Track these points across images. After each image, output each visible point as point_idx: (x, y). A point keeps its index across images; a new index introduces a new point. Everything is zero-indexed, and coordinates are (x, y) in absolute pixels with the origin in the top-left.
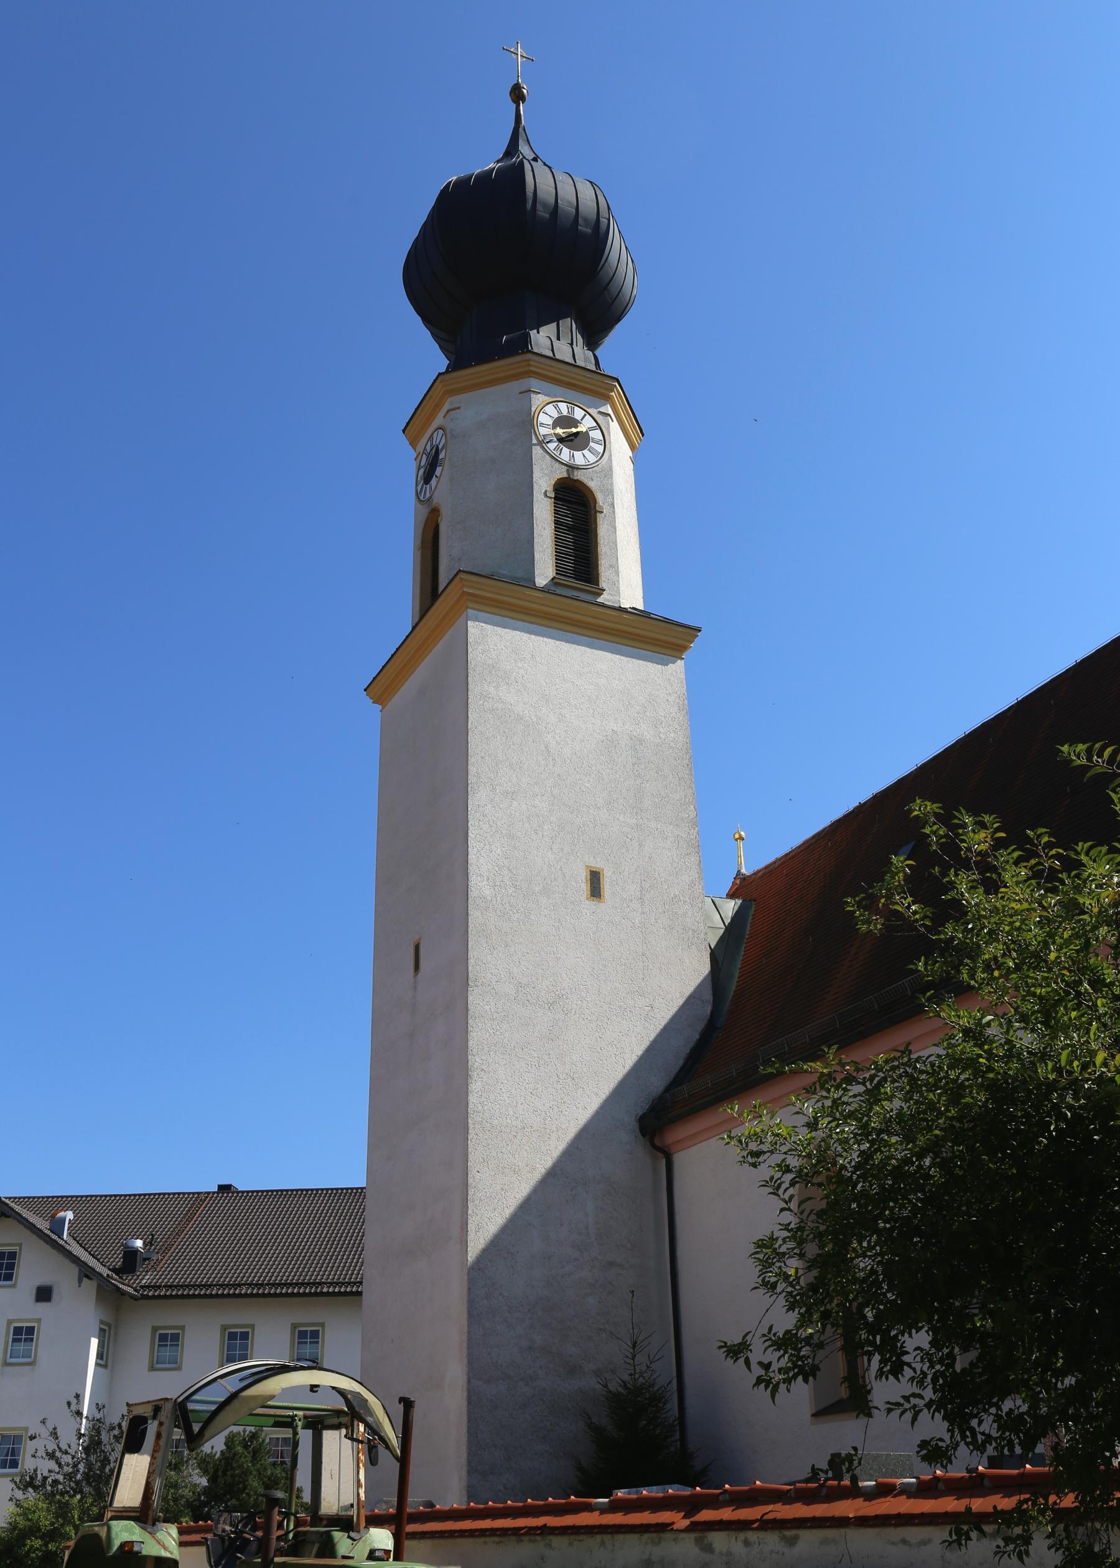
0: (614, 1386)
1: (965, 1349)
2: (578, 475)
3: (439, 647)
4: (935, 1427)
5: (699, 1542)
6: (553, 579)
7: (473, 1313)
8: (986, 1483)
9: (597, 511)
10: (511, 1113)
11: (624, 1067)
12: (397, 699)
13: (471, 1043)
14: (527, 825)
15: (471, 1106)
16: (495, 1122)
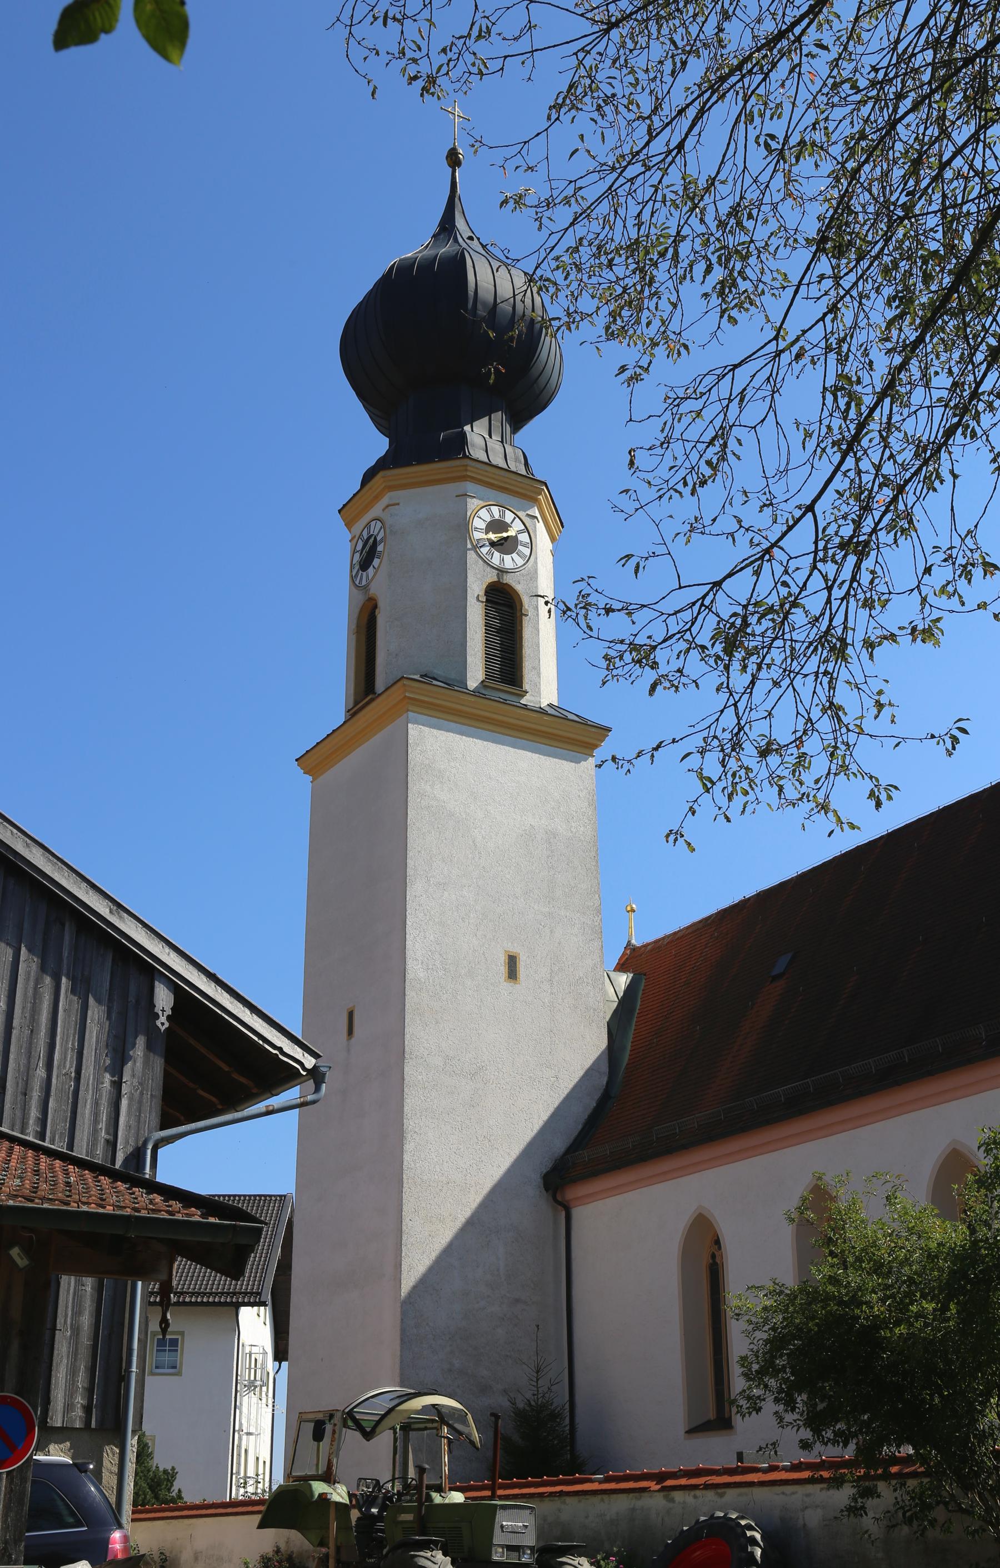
0: (521, 1405)
1: (822, 1401)
2: (508, 579)
3: (377, 740)
4: (807, 1434)
5: (666, 1497)
6: (482, 682)
7: (405, 1341)
8: (826, 1465)
9: (522, 614)
10: (439, 1170)
11: (532, 1131)
12: (330, 775)
13: (406, 1108)
14: (455, 913)
15: (405, 1163)
16: (425, 1178)
